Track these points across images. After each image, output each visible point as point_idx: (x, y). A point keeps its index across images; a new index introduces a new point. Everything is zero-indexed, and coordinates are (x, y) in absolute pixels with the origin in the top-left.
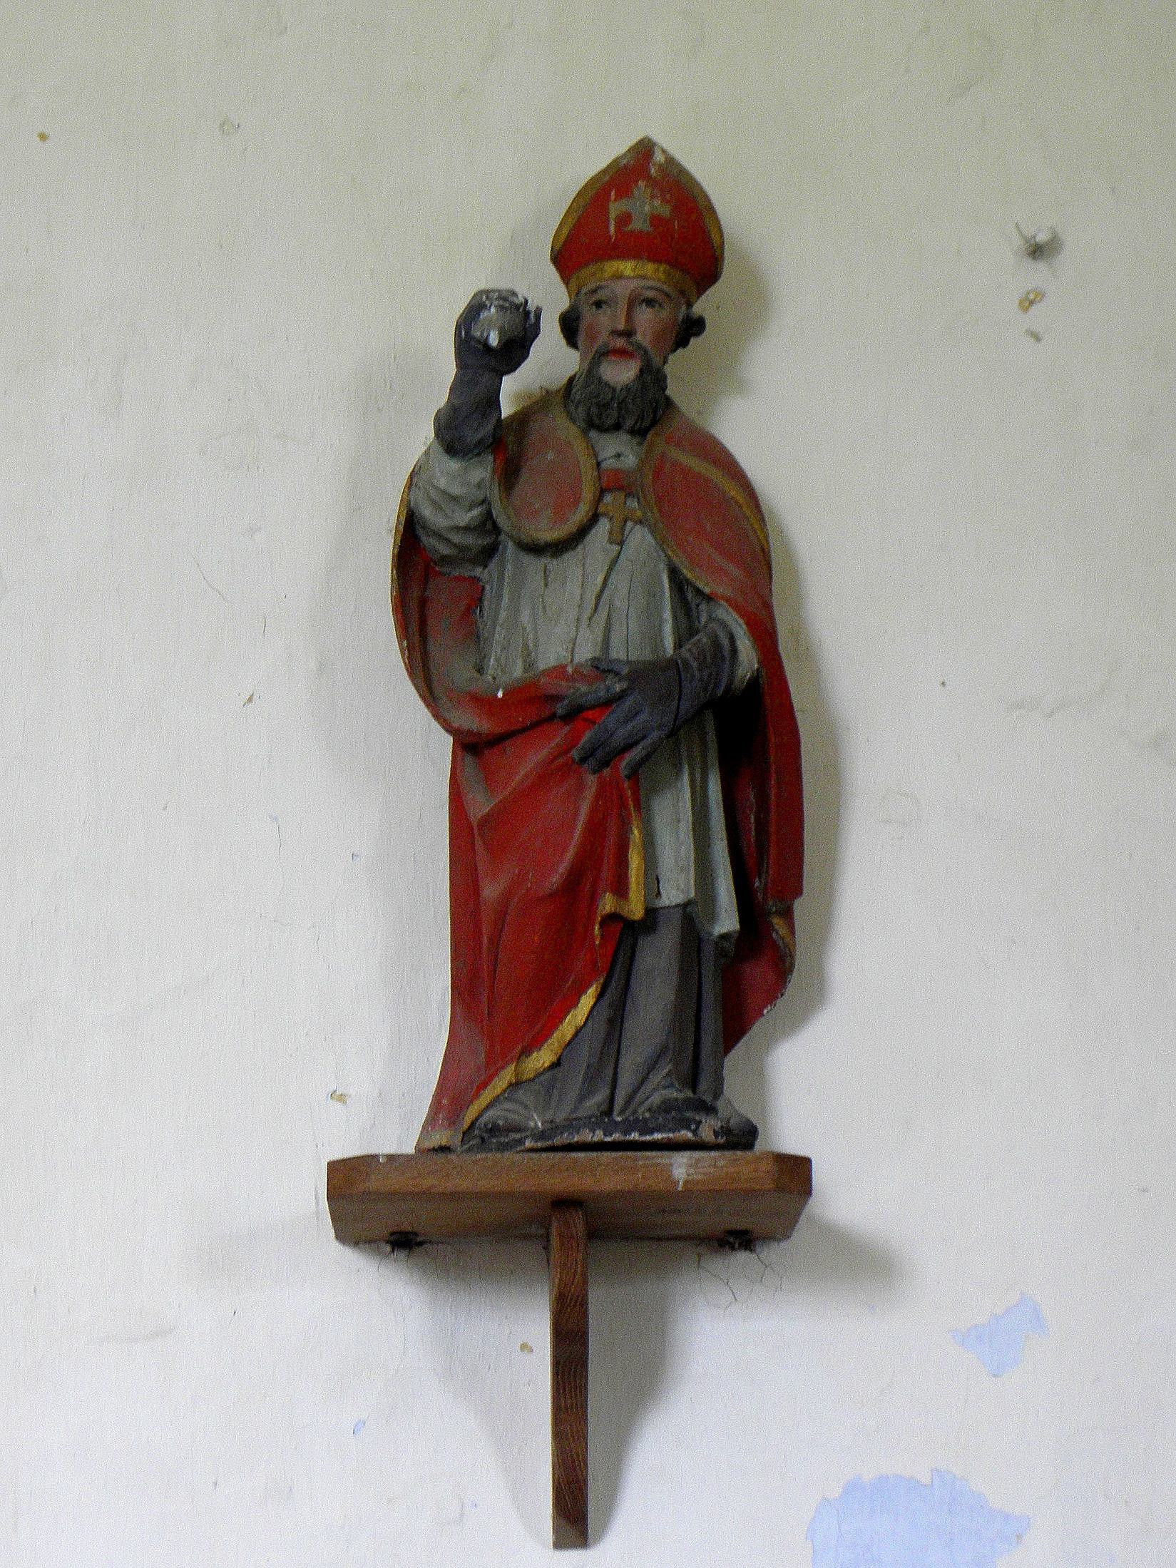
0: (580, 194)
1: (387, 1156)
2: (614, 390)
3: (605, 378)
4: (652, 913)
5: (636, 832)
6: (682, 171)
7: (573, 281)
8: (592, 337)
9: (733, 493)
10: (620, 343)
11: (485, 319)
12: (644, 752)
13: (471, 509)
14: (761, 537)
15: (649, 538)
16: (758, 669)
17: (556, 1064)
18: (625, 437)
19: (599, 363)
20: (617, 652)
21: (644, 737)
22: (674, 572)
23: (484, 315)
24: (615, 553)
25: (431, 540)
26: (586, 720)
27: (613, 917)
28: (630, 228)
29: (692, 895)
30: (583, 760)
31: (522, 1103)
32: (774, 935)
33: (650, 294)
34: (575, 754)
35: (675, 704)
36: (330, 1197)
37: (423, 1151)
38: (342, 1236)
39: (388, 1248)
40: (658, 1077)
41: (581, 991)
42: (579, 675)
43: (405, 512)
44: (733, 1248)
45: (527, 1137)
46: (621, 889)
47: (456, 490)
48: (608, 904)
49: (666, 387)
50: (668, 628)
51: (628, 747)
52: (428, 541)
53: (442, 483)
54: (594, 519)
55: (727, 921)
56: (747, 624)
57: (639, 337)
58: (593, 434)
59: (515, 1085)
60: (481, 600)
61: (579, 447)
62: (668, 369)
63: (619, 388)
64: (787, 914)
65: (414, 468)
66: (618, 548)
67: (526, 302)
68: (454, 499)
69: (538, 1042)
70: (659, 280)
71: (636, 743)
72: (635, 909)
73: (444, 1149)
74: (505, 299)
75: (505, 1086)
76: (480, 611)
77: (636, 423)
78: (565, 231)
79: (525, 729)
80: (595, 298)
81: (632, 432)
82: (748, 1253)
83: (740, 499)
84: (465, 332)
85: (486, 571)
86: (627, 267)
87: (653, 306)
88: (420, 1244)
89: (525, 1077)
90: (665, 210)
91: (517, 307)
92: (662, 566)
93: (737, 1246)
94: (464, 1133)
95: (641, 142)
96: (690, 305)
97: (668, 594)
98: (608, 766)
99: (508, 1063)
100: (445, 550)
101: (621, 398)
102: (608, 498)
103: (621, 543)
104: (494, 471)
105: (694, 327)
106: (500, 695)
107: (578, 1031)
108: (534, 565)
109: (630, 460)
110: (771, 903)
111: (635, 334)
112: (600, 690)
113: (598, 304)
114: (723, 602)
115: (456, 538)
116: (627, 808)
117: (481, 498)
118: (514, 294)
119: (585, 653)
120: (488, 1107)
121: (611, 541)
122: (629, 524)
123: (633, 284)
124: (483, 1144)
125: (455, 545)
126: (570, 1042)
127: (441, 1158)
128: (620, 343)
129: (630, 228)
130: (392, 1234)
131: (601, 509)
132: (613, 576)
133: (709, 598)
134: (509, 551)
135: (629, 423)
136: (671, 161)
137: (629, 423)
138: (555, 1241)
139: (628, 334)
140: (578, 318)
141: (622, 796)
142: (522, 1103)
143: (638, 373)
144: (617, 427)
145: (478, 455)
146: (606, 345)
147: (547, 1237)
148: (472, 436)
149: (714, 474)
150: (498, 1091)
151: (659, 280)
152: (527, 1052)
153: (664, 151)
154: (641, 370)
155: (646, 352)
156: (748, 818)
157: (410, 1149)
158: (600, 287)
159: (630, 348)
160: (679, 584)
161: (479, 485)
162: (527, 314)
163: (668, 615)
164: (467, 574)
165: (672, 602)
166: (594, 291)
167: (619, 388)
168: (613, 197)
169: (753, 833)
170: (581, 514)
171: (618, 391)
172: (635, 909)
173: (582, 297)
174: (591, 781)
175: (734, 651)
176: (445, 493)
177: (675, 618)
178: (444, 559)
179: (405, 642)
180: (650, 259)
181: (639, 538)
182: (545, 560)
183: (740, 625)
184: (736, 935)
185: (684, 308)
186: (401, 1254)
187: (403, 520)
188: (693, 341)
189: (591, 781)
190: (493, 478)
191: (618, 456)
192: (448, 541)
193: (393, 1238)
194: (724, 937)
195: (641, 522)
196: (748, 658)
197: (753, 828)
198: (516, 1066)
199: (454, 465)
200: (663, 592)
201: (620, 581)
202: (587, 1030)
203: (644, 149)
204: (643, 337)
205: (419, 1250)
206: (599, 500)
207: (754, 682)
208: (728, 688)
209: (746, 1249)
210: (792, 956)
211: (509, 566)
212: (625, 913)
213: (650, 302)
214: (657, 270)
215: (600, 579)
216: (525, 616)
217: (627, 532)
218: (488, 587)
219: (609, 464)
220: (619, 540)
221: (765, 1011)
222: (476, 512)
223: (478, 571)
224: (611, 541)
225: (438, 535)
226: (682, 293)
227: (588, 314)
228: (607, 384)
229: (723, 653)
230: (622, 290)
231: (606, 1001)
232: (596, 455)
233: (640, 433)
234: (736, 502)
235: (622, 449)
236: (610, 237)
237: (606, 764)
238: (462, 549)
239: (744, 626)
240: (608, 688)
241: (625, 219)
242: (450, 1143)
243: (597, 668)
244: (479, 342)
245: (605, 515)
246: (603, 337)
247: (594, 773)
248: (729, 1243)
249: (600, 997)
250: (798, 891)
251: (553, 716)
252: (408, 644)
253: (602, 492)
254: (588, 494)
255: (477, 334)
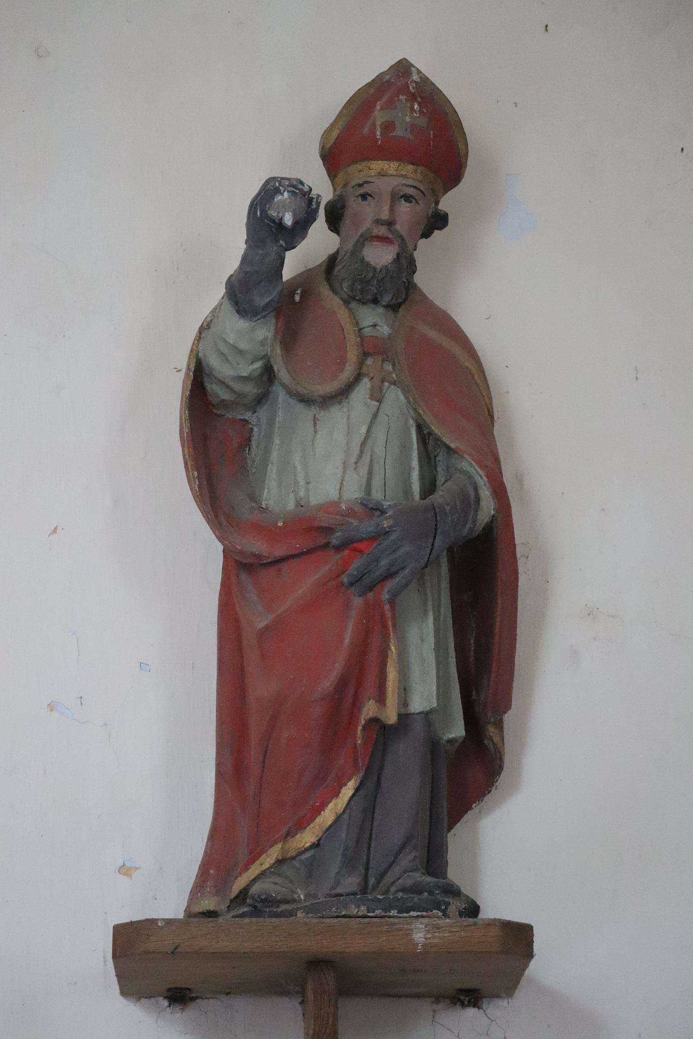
1: (164, 920)
2: (375, 269)
3: (367, 259)
4: (404, 718)
5: (393, 648)
7: (341, 176)
9: (467, 364)
10: (382, 231)
11: (279, 201)
13: (252, 363)
16: (493, 516)
17: (316, 846)
18: (381, 310)
19: (363, 245)
20: (377, 495)
22: (419, 428)
26: (355, 550)
27: (375, 721)
28: (394, 134)
29: (435, 705)
30: (352, 584)
31: (286, 877)
32: (486, 742)
33: (410, 191)
34: (345, 579)
35: (431, 540)
36: (114, 957)
37: (190, 914)
38: (125, 991)
39: (166, 1003)
40: (406, 860)
41: (341, 785)
42: (350, 512)
44: (463, 1005)
45: (298, 909)
46: (381, 699)
47: (243, 345)
48: (370, 709)
49: (416, 270)
50: (415, 475)
52: (212, 388)
53: (231, 339)
54: (358, 378)
55: (457, 730)
56: (488, 476)
57: (398, 227)
58: (353, 305)
59: (280, 862)
62: (416, 254)
63: (379, 267)
64: (499, 725)
65: (202, 324)
66: (378, 404)
67: (311, 189)
68: (241, 352)
69: (301, 825)
72: (391, 716)
73: (211, 914)
74: (294, 187)
75: (272, 862)
77: (393, 298)
78: (335, 134)
79: (303, 553)
80: (362, 191)
81: (387, 307)
82: (476, 1010)
85: (255, 415)
86: (391, 167)
87: (411, 202)
88: (192, 999)
89: (289, 855)
90: (423, 121)
92: (411, 422)
93: (466, 1003)
94: (231, 901)
95: (400, 62)
96: (437, 203)
97: (415, 446)
98: (371, 590)
99: (276, 842)
100: (225, 395)
102: (369, 361)
103: (380, 401)
104: (276, 332)
105: (439, 221)
106: (280, 524)
107: (338, 819)
108: (304, 414)
109: (385, 330)
110: (489, 714)
112: (367, 527)
113: (364, 197)
115: (237, 386)
116: (388, 629)
118: (302, 183)
119: (353, 492)
120: (255, 880)
122: (386, 384)
123: (396, 182)
124: (256, 912)
126: (330, 826)
127: (209, 923)
128: (382, 231)
129: (394, 134)
130: (169, 990)
131: (364, 370)
134: (280, 400)
135: (386, 299)
136: (425, 80)
137: (386, 299)
138: (310, 996)
139: (390, 224)
140: (344, 207)
141: (383, 615)
142: (286, 877)
144: (375, 301)
145: (265, 317)
147: (303, 993)
148: (261, 301)
149: (456, 350)
150: (266, 866)
152: (290, 834)
153: (419, 72)
154: (398, 255)
155: (403, 239)
157: (181, 916)
158: (367, 182)
159: (390, 236)
160: (425, 436)
161: (262, 343)
162: (310, 200)
163: (415, 463)
166: (360, 185)
167: (379, 267)
169: (472, 653)
170: (349, 371)
171: (378, 271)
172: (391, 716)
173: (349, 188)
174: (357, 602)
175: (478, 500)
176: (234, 347)
181: (394, 397)
182: (314, 410)
183: (482, 478)
184: (461, 740)
185: (433, 205)
186: (177, 1008)
187: (192, 367)
189: (357, 602)
190: (275, 336)
191: (375, 326)
193: (170, 994)
194: (451, 741)
195: (395, 384)
196: (488, 506)
198: (283, 845)
199: (243, 324)
201: (380, 434)
202: (346, 816)
203: (403, 68)
204: (401, 227)
205: (193, 1005)
206: (361, 363)
207: (489, 529)
208: (471, 530)
209: (474, 1006)
210: (501, 760)
212: (383, 718)
213: (408, 198)
214: (416, 171)
215: (364, 430)
216: (297, 458)
217: (384, 391)
218: (255, 429)
219: (368, 332)
220: (378, 396)
221: (474, 806)
222: (258, 365)
223: (247, 416)
225: (222, 383)
227: (354, 205)
228: (368, 264)
229: (470, 503)
230: (385, 186)
231: (362, 793)
233: (394, 307)
236: (377, 140)
238: (242, 395)
239: (485, 479)
241: (388, 126)
242: (217, 909)
243: (365, 505)
244: (273, 221)
245: (367, 375)
246: (367, 224)
247: (360, 596)
248: (459, 1000)
249: (357, 790)
250: (508, 706)
251: (327, 545)
253: (366, 355)
254: (352, 355)
255: (273, 213)
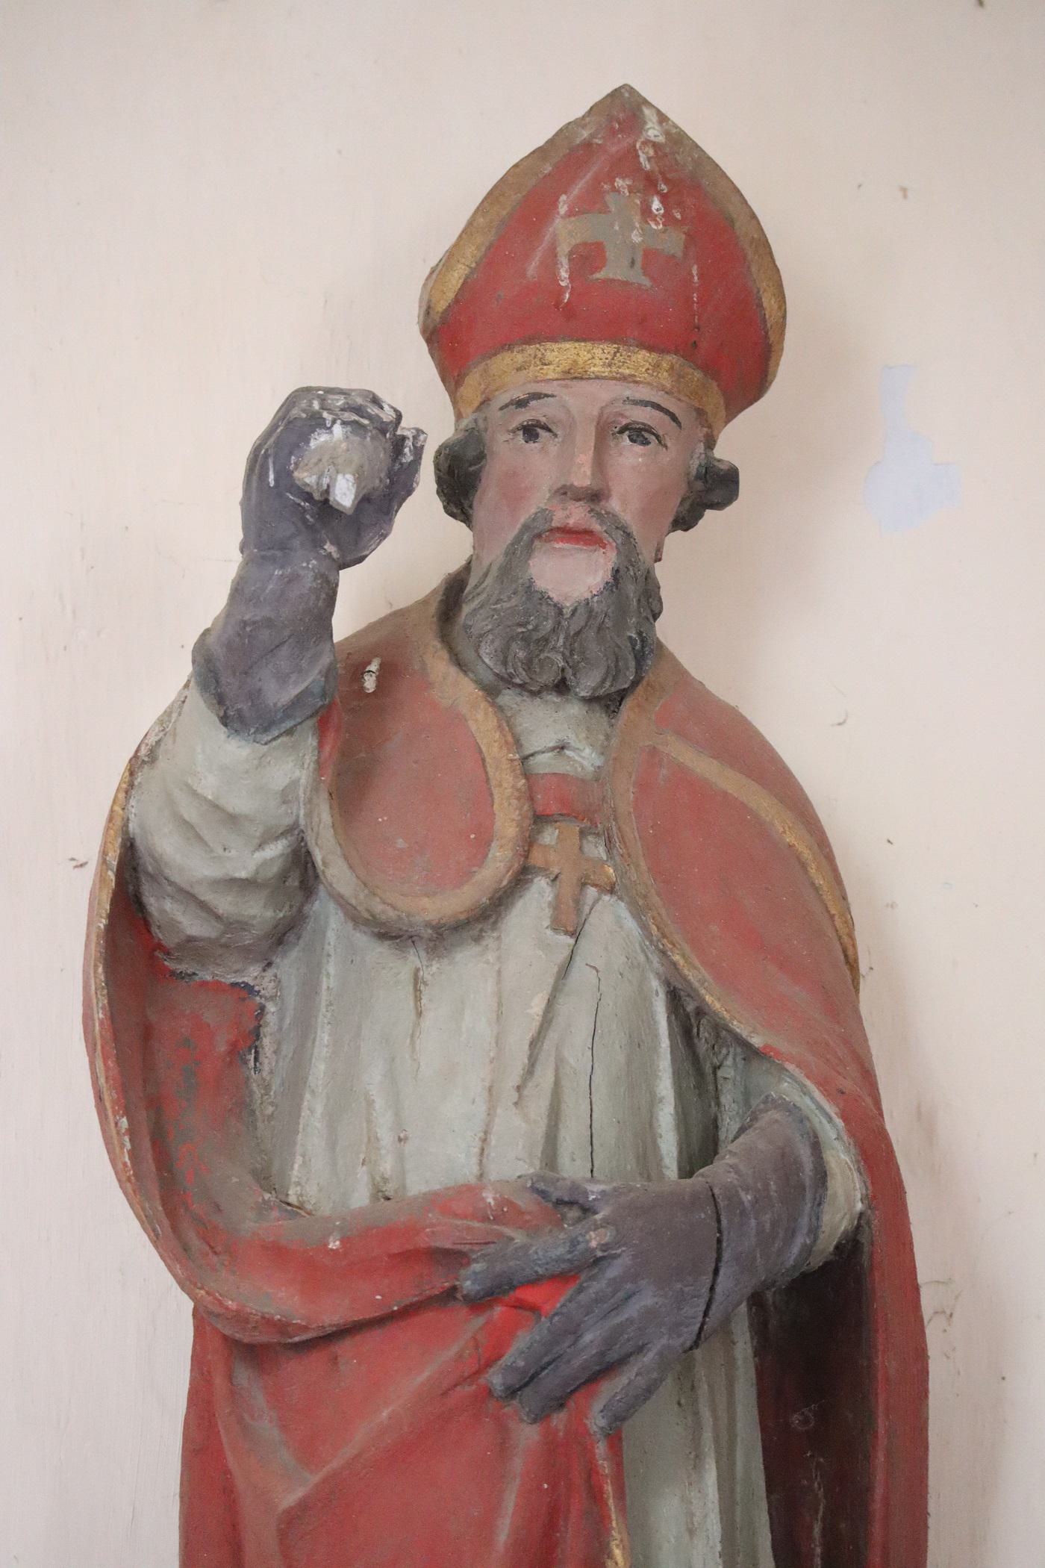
0: (494, 196)
2: (560, 611)
3: (541, 584)
5: (617, 1553)
6: (703, 160)
8: (515, 496)
9: (789, 838)
10: (577, 515)
11: (320, 448)
12: (641, 1382)
14: (843, 931)
15: (630, 924)
16: (861, 1215)
18: (575, 709)
19: (529, 550)
20: (572, 1167)
21: (640, 1349)
22: (675, 998)
23: (319, 440)
24: (566, 953)
25: (168, 905)
28: (600, 275)
30: (512, 1392)
34: (496, 1379)
35: (707, 1279)
42: (506, 1213)
43: (120, 840)
47: (239, 803)
51: (605, 1369)
52: (161, 906)
53: (209, 785)
54: (522, 877)
57: (614, 504)
60: (256, 1034)
61: (482, 723)
62: (660, 571)
66: (572, 941)
67: (399, 416)
68: (232, 820)
70: (663, 389)
71: (623, 1361)
74: (358, 410)
76: (256, 1059)
77: (603, 681)
78: (455, 279)
80: (524, 416)
81: (591, 700)
83: (807, 854)
84: (276, 473)
85: (270, 973)
86: (594, 356)
90: (673, 243)
91: (382, 429)
92: (655, 984)
95: (615, 94)
96: (710, 443)
97: (665, 1043)
100: (193, 925)
101: (574, 629)
102: (549, 836)
103: (576, 934)
104: (320, 767)
109: (586, 758)
111: (608, 497)
113: (530, 431)
114: (790, 1067)
115: (225, 904)
117: (288, 821)
118: (376, 401)
121: (557, 925)
125: (218, 918)
129: (600, 275)
131: (537, 858)
132: (561, 999)
133: (751, 1054)
135: (588, 682)
136: (678, 139)
137: (588, 682)
139: (595, 497)
140: (481, 457)
143: (609, 577)
144: (562, 687)
145: (289, 732)
146: (545, 514)
149: (761, 802)
151: (663, 389)
153: (662, 118)
154: (616, 572)
156: (811, 1528)
158: (537, 396)
159: (597, 527)
161: (286, 797)
163: (665, 1087)
164: (232, 979)
165: (674, 1060)
168: (563, 209)
171: (567, 612)
174: (527, 1435)
175: (822, 1176)
177: (680, 1095)
178: (191, 946)
179: (124, 1120)
180: (642, 345)
182: (414, 958)
183: (830, 1120)
185: (701, 448)
188: (710, 517)
191: (561, 748)
192: (203, 906)
195: (612, 890)
197: (818, 1550)
199: (236, 750)
200: (656, 1036)
206: (528, 843)
207: (850, 1248)
211: (331, 968)
213: (639, 433)
214: (657, 366)
215: (537, 1006)
216: (373, 1079)
217: (587, 909)
218: (271, 1008)
222: (276, 850)
223: (251, 974)
224: (557, 925)
225: (187, 896)
226: (700, 413)
228: (544, 598)
232: (518, 743)
233: (609, 702)
234: (798, 858)
235: (572, 739)
236: (561, 290)
237: (561, 1404)
238: (234, 925)
240: (574, 1243)
241: (588, 257)
243: (543, 1194)
245: (544, 870)
246: (539, 499)
247: (534, 1421)
251: (451, 1293)
252: (130, 1124)
253: (540, 819)
254: (507, 822)
255: (306, 477)
